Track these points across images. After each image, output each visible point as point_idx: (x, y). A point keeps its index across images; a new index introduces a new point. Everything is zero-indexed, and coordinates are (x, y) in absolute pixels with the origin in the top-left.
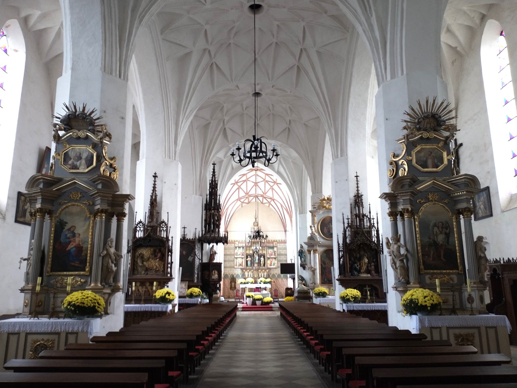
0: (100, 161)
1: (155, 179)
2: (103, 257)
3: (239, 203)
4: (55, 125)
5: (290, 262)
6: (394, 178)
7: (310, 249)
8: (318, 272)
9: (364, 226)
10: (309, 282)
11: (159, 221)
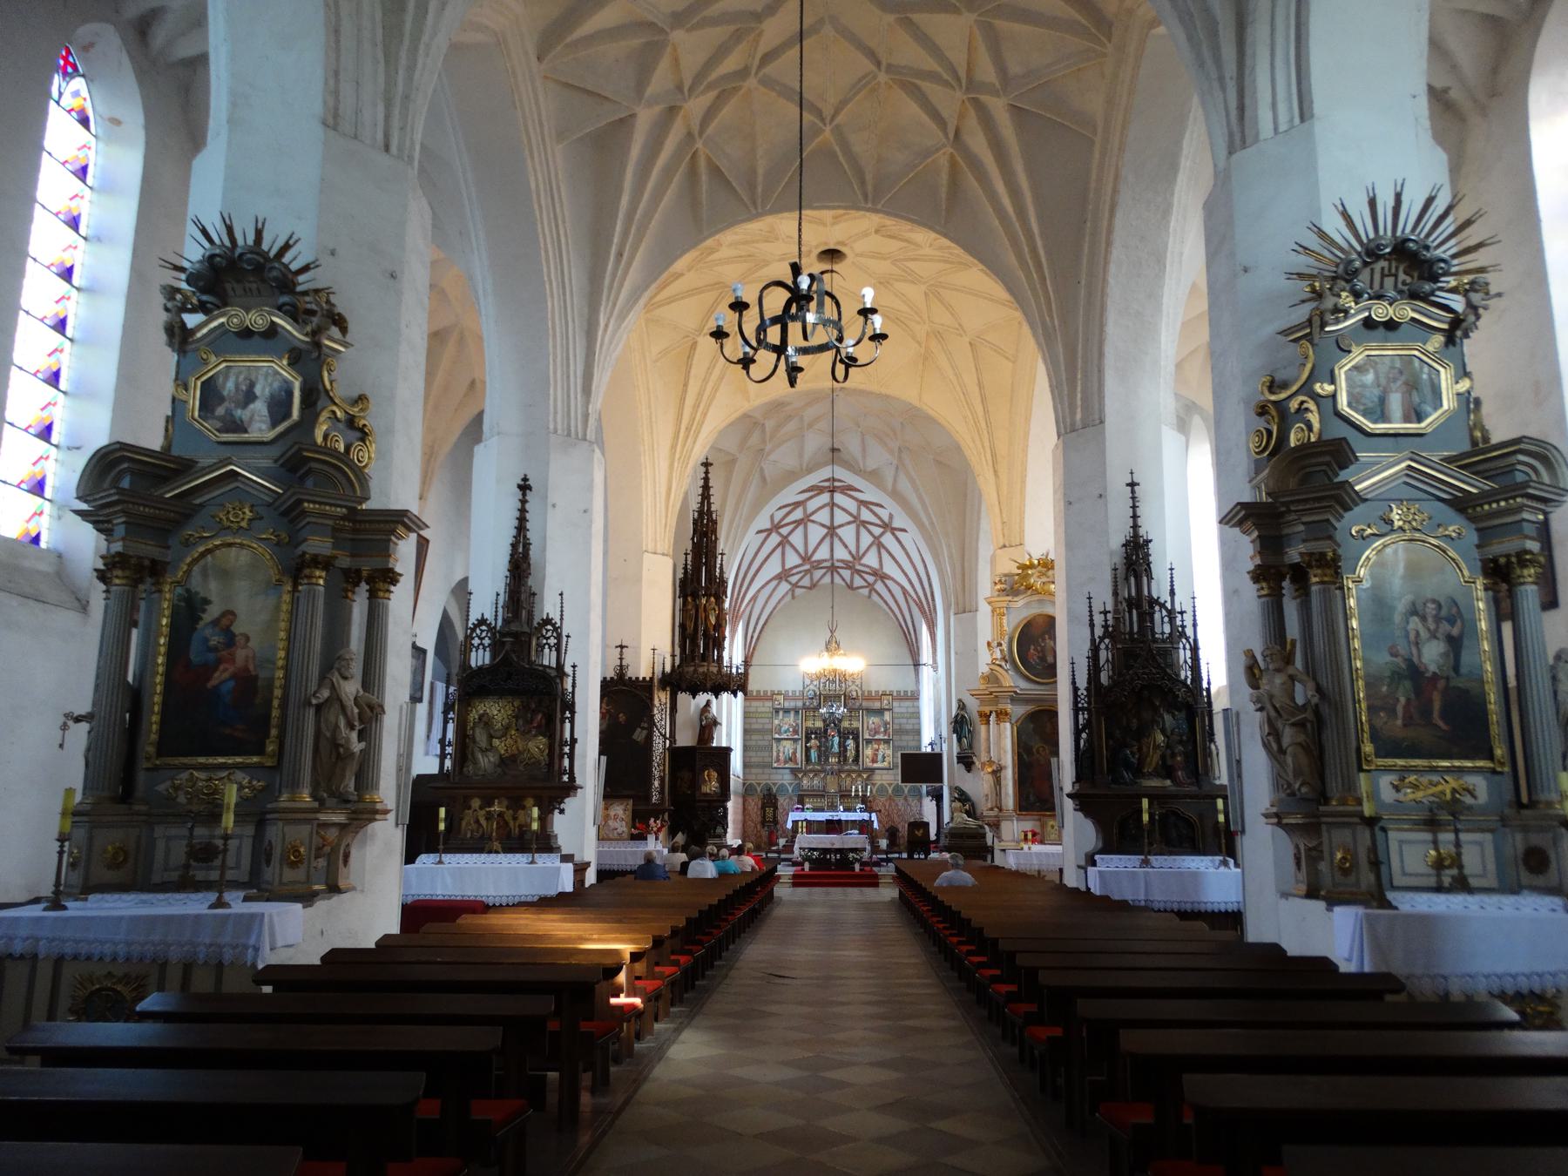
0: (315, 404)
1: (524, 495)
2: (319, 708)
3: (784, 587)
4: (171, 292)
5: (929, 750)
6: (1272, 455)
7: (987, 709)
8: (1009, 776)
9: (1153, 633)
10: (984, 807)
11: (537, 620)
